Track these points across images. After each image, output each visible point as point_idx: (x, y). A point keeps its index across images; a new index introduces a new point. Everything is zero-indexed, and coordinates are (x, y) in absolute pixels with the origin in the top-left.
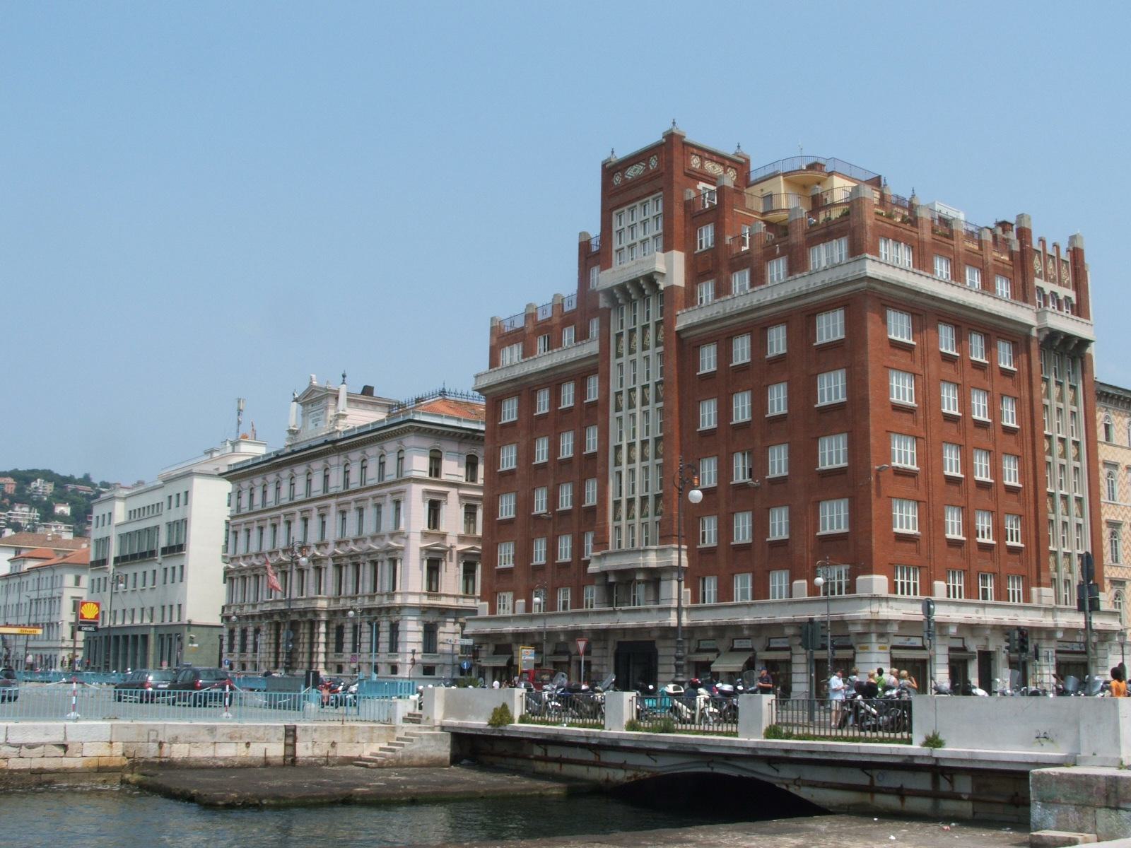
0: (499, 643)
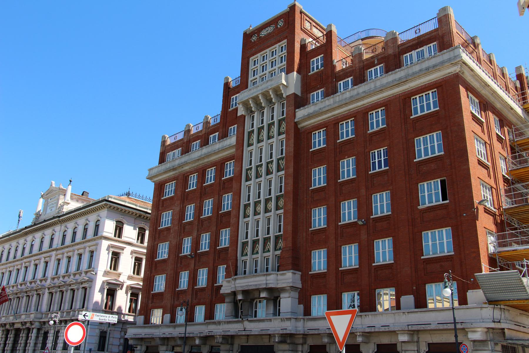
0: (149, 345)
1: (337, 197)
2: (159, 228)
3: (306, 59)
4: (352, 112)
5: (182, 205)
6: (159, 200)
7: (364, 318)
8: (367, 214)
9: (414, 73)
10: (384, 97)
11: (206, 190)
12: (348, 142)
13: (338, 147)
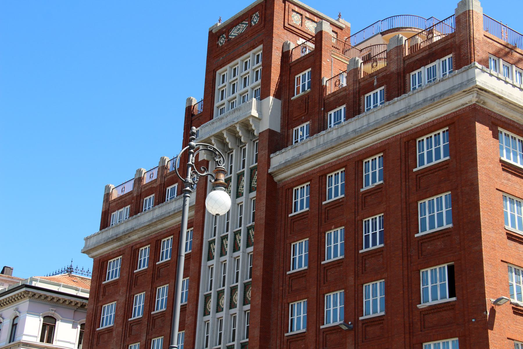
2: (98, 329)
4: (341, 159)
6: (100, 285)
8: (355, 313)
9: (416, 105)
10: (380, 139)
11: (161, 271)
13: (323, 211)
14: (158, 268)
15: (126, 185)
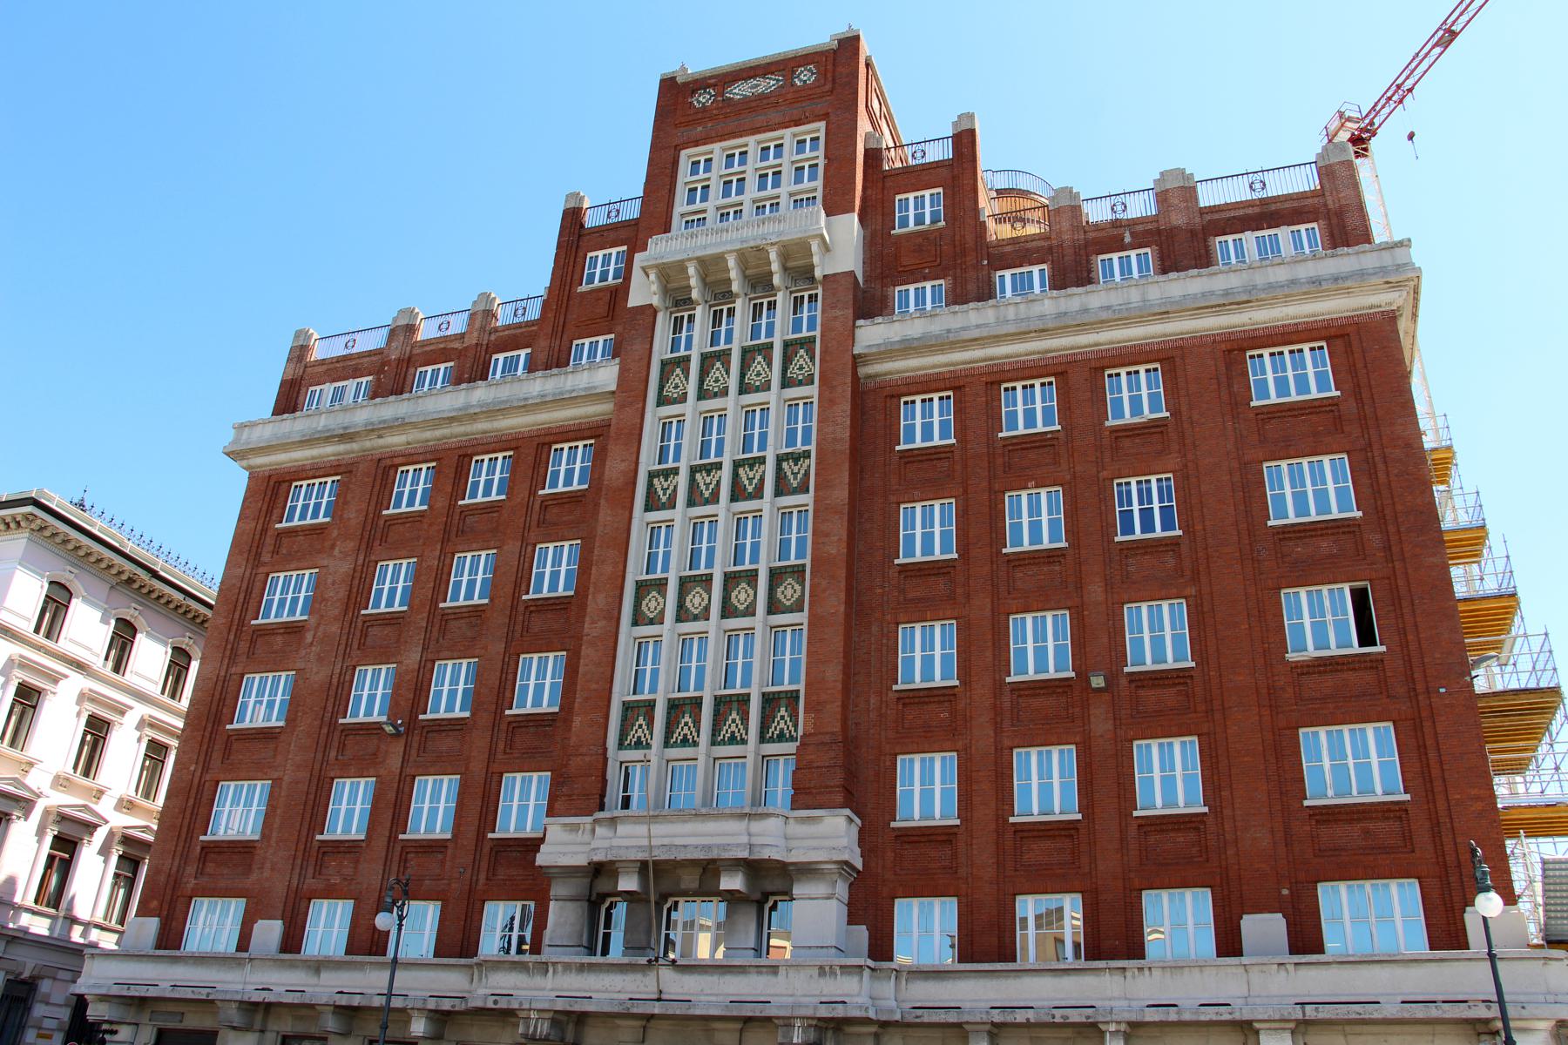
1: (999, 599)
3: (883, 189)
5: (361, 558)
7: (1134, 977)
9: (1271, 287)
10: (1166, 336)
12: (1034, 442)
14: (461, 512)
15: (451, 318)
